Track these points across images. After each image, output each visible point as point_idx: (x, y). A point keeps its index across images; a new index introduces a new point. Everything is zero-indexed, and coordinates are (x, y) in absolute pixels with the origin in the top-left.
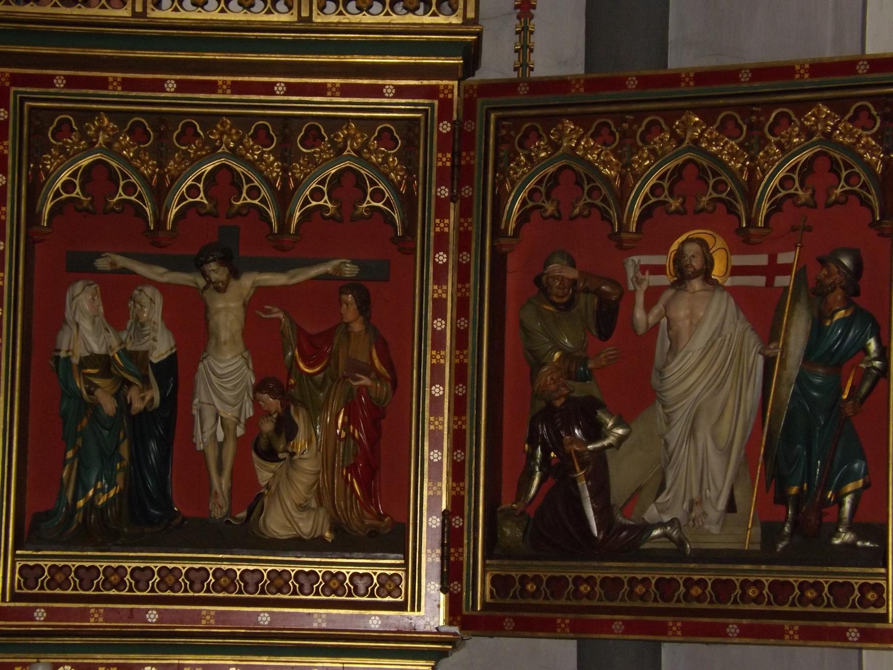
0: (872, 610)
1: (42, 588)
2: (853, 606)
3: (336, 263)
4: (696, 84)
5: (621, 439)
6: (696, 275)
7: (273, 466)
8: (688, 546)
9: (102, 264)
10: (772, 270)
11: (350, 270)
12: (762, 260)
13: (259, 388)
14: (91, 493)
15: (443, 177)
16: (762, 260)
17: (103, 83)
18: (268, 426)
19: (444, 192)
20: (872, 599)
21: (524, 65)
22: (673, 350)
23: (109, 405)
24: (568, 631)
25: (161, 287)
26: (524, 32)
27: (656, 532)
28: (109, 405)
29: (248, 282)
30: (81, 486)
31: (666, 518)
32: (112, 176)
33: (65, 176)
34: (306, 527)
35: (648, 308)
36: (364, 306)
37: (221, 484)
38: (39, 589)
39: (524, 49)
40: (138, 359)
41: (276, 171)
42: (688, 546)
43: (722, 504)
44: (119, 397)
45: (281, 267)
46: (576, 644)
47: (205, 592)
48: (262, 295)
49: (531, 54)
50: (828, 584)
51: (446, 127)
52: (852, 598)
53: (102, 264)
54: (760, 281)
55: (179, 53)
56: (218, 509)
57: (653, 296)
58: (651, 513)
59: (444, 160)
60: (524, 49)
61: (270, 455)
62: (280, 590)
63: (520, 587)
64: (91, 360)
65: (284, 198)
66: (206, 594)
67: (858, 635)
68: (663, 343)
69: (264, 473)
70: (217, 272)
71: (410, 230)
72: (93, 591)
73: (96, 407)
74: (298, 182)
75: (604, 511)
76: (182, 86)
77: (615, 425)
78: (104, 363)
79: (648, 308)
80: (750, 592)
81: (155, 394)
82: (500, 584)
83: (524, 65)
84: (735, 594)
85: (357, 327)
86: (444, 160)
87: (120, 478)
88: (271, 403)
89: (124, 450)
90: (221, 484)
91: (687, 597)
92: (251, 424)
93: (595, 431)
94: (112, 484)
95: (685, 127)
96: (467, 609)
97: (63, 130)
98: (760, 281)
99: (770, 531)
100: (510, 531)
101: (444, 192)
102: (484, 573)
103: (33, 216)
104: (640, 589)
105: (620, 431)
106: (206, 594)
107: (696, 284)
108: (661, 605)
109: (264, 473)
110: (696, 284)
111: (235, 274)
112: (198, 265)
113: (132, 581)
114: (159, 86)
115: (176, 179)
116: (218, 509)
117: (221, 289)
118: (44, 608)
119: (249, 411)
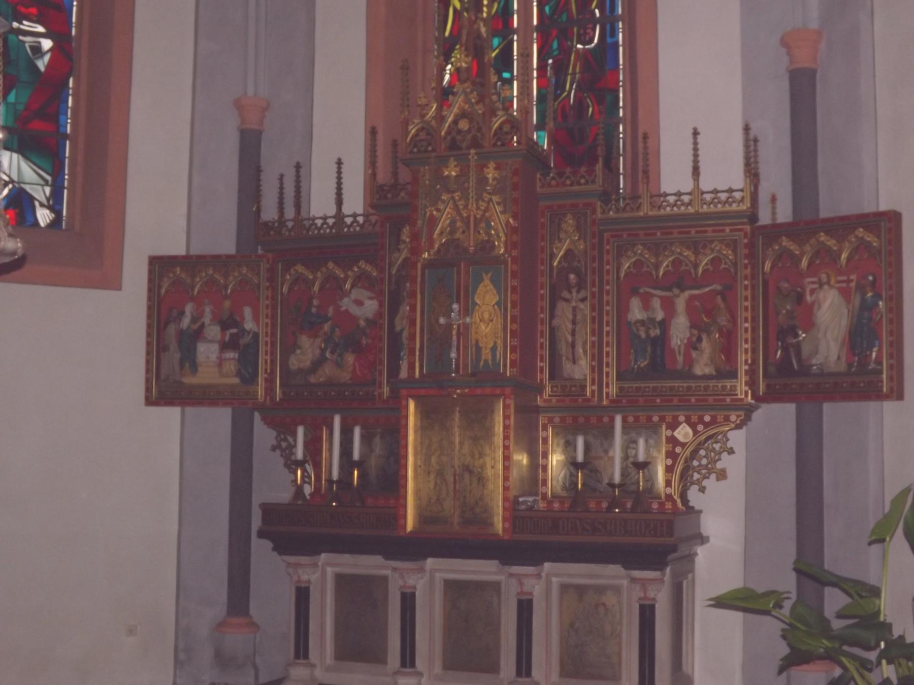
0: (733, 393)
3: (715, 285)
5: (804, 338)
6: (825, 284)
7: (697, 352)
9: (641, 291)
10: (849, 281)
11: (718, 287)
12: (845, 278)
13: (691, 327)
14: (639, 363)
15: (746, 256)
16: (845, 278)
17: (706, 232)
18: (694, 339)
19: (746, 261)
21: (774, 219)
22: (819, 307)
23: (643, 335)
25: (660, 297)
26: (774, 208)
27: (815, 368)
28: (643, 335)
29: (687, 294)
30: (636, 361)
31: (818, 363)
32: (681, 262)
33: (705, 262)
34: (708, 370)
35: (811, 294)
36: (724, 299)
37: (680, 359)
39: (774, 213)
40: (652, 320)
41: (693, 258)
43: (836, 357)
44: (647, 333)
45: (698, 288)
46: (228, 422)
48: (692, 298)
51: (746, 241)
53: (641, 291)
54: (844, 285)
56: (679, 366)
57: (813, 292)
58: (814, 361)
59: (746, 251)
60: (774, 213)
61: (696, 349)
62: (699, 391)
64: (638, 321)
65: (696, 266)
68: (816, 306)
69: (694, 354)
70: (676, 291)
71: (736, 273)
73: (639, 337)
74: (700, 261)
75: (799, 360)
76: (697, 232)
77: (803, 333)
78: (642, 322)
79: (811, 294)
81: (658, 331)
82: (768, 386)
83: (774, 219)
85: (722, 306)
86: (746, 251)
87: (648, 358)
88: (696, 332)
89: (649, 349)
90: (680, 359)
91: (713, 390)
92: (689, 339)
93: (796, 335)
94: (645, 359)
95: (820, 237)
97: (705, 247)
98: (844, 285)
99: (850, 365)
100: (772, 369)
101: (746, 261)
102: (616, 385)
103: (618, 278)
104: (664, 389)
105: (804, 335)
107: (826, 287)
108: (705, 393)
109: (694, 354)
110: (826, 287)
111: (682, 291)
112: (669, 289)
114: (655, 234)
115: (662, 262)
116: (679, 366)
117: (678, 296)
119: (688, 335)
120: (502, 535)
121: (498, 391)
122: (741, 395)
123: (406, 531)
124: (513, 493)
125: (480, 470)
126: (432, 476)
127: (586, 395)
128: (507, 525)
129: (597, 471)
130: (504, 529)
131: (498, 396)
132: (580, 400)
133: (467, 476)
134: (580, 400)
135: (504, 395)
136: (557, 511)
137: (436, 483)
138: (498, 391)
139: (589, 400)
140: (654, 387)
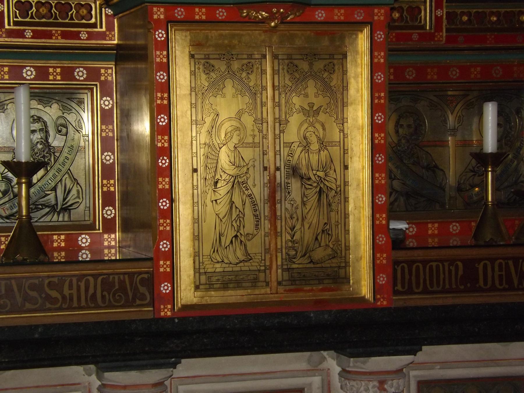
1: (32, 17)
2: (32, 17)
4: (72, 290)
8: (488, 34)
20: (43, 13)
24: (60, 38)
38: (69, 20)
42: (488, 34)
47: (30, 18)
49: (265, 156)
50: (74, 4)
52: (32, 11)
55: (120, 218)
63: (75, 12)
66: (31, 20)
67: (25, 34)
72: (69, 20)
80: (85, 12)
84: (32, 11)
96: (9, 24)
106: (31, 20)
113: (407, 15)
118: (417, 33)
120: (371, 300)
121: (359, 16)
122: (101, 27)
123: (138, 299)
124: (34, 198)
125: (321, 174)
126: (223, 189)
127: (423, 27)
128: (382, 279)
129: (436, 166)
130: (376, 288)
131: (362, 24)
132: (415, 37)
133: (295, 185)
134: (415, 37)
135: (371, 24)
136: (433, 248)
137: (232, 203)
138: (359, 16)
139: (430, 36)
140: (477, 12)
